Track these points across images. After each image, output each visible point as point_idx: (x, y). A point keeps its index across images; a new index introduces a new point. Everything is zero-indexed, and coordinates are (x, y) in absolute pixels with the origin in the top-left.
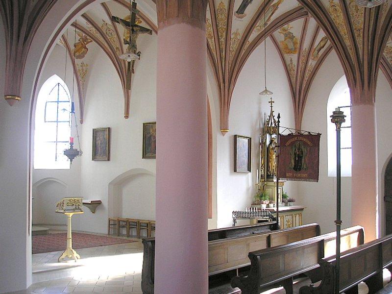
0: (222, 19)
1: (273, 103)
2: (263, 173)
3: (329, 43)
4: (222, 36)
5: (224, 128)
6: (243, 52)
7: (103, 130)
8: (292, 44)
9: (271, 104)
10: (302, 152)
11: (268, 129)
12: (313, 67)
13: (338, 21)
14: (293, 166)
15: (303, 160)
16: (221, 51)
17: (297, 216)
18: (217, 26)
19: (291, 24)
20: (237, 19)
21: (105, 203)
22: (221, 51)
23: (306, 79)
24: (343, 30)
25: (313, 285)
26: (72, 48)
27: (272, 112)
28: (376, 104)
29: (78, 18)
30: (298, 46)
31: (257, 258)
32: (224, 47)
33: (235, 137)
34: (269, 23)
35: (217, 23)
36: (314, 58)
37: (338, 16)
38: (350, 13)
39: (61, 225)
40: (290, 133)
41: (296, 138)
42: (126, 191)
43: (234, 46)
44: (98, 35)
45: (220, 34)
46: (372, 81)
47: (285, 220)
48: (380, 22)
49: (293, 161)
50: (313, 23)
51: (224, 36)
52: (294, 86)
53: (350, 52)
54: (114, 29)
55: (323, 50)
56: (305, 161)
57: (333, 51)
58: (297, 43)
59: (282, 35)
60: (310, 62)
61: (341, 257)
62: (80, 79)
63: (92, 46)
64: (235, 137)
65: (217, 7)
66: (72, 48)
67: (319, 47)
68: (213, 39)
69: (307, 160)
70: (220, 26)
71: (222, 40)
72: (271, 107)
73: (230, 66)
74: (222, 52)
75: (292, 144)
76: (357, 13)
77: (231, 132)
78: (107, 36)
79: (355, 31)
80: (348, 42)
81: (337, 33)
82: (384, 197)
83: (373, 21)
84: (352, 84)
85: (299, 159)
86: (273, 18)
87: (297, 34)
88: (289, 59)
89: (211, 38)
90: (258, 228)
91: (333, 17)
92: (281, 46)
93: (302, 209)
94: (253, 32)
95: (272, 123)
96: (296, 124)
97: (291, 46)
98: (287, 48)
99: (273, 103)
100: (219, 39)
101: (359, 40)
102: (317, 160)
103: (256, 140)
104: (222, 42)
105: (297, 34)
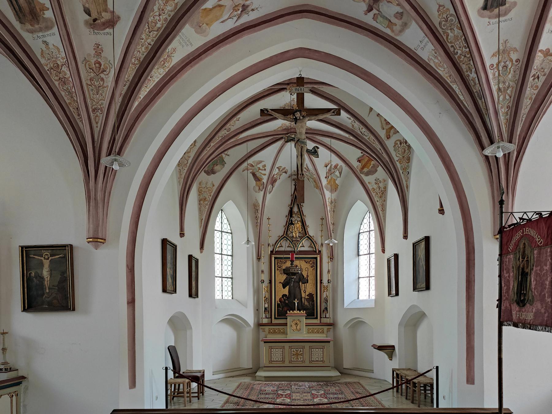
26: (356, 164)
58: (223, 163)
62: (376, 199)
66: (356, 164)
78: (364, 137)
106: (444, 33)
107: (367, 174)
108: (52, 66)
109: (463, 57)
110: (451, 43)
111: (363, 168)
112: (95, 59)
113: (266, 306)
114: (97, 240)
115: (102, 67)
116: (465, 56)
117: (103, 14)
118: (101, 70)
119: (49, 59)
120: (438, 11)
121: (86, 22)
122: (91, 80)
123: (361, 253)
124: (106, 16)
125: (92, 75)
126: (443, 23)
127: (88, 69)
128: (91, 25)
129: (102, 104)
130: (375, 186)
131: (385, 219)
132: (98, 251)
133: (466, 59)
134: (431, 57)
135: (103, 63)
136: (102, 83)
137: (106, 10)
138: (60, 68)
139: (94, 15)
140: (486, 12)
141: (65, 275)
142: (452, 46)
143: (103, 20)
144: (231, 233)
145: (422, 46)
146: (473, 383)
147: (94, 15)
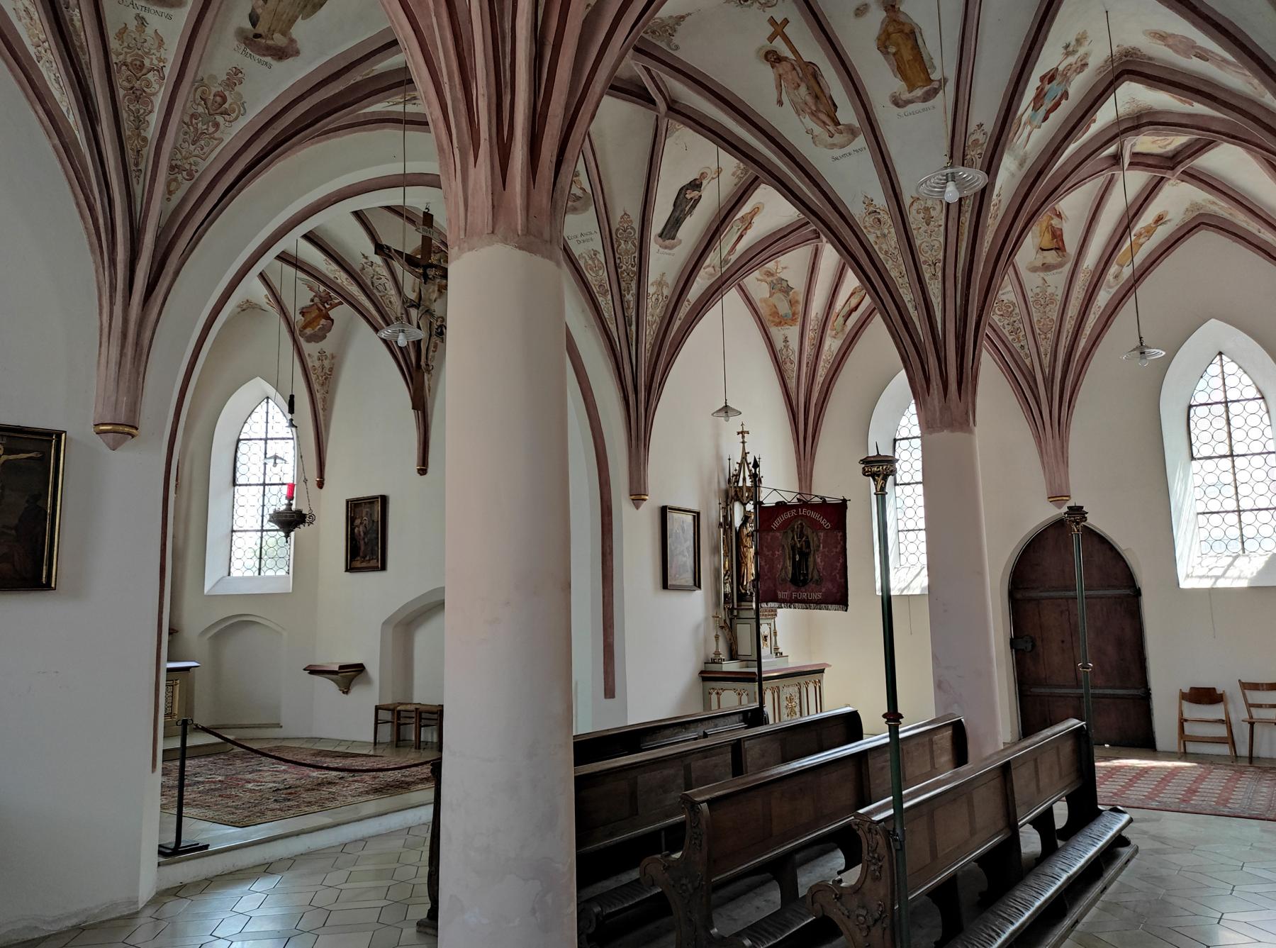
0: (627, 252)
2: (728, 590)
3: (867, 300)
5: (638, 496)
6: (677, 324)
7: (370, 501)
8: (786, 304)
10: (808, 543)
13: (884, 247)
15: (811, 559)
16: (627, 323)
19: (784, 260)
21: (373, 670)
23: (820, 379)
24: (896, 268)
25: (840, 881)
26: (299, 319)
27: (745, 454)
28: (976, 430)
29: (294, 242)
30: (800, 308)
31: (700, 811)
33: (664, 511)
34: (733, 258)
37: (884, 236)
38: (913, 226)
39: (260, 726)
41: (793, 512)
42: (423, 638)
43: (653, 312)
44: (354, 289)
45: (623, 284)
46: (966, 380)
47: (783, 697)
48: (980, 255)
49: (789, 564)
50: (830, 256)
51: (634, 291)
52: (793, 396)
53: (914, 314)
54: (389, 277)
56: (818, 560)
57: (878, 319)
58: (797, 302)
61: (901, 736)
62: (316, 387)
63: (341, 313)
64: (664, 511)
66: (299, 319)
67: (847, 309)
68: (609, 297)
69: (819, 560)
71: (630, 297)
75: (786, 525)
79: (924, 267)
80: (908, 296)
83: (968, 215)
84: (920, 391)
85: (802, 555)
86: (741, 247)
87: (797, 281)
88: (782, 339)
89: (604, 294)
90: (716, 721)
91: (872, 238)
92: (764, 311)
95: (744, 479)
96: (800, 480)
97: (784, 308)
100: (621, 296)
101: (934, 289)
103: (712, 514)
104: (628, 302)
105: (797, 281)
107: (309, 339)
108: (129, 60)
111: (305, 327)
112: (221, 89)
114: (122, 430)
115: (226, 105)
117: (277, 36)
118: (222, 109)
119: (129, 47)
121: (241, 33)
122: (193, 116)
123: (240, 480)
124: (279, 40)
125: (201, 110)
127: (198, 96)
128: (246, 38)
129: (196, 164)
130: (317, 364)
131: (327, 426)
132: (119, 454)
135: (229, 101)
136: (211, 130)
137: (284, 33)
138: (144, 71)
139: (261, 29)
141: (40, 503)
143: (270, 42)
144: (1263, 398)
146: (613, 696)
147: (261, 29)
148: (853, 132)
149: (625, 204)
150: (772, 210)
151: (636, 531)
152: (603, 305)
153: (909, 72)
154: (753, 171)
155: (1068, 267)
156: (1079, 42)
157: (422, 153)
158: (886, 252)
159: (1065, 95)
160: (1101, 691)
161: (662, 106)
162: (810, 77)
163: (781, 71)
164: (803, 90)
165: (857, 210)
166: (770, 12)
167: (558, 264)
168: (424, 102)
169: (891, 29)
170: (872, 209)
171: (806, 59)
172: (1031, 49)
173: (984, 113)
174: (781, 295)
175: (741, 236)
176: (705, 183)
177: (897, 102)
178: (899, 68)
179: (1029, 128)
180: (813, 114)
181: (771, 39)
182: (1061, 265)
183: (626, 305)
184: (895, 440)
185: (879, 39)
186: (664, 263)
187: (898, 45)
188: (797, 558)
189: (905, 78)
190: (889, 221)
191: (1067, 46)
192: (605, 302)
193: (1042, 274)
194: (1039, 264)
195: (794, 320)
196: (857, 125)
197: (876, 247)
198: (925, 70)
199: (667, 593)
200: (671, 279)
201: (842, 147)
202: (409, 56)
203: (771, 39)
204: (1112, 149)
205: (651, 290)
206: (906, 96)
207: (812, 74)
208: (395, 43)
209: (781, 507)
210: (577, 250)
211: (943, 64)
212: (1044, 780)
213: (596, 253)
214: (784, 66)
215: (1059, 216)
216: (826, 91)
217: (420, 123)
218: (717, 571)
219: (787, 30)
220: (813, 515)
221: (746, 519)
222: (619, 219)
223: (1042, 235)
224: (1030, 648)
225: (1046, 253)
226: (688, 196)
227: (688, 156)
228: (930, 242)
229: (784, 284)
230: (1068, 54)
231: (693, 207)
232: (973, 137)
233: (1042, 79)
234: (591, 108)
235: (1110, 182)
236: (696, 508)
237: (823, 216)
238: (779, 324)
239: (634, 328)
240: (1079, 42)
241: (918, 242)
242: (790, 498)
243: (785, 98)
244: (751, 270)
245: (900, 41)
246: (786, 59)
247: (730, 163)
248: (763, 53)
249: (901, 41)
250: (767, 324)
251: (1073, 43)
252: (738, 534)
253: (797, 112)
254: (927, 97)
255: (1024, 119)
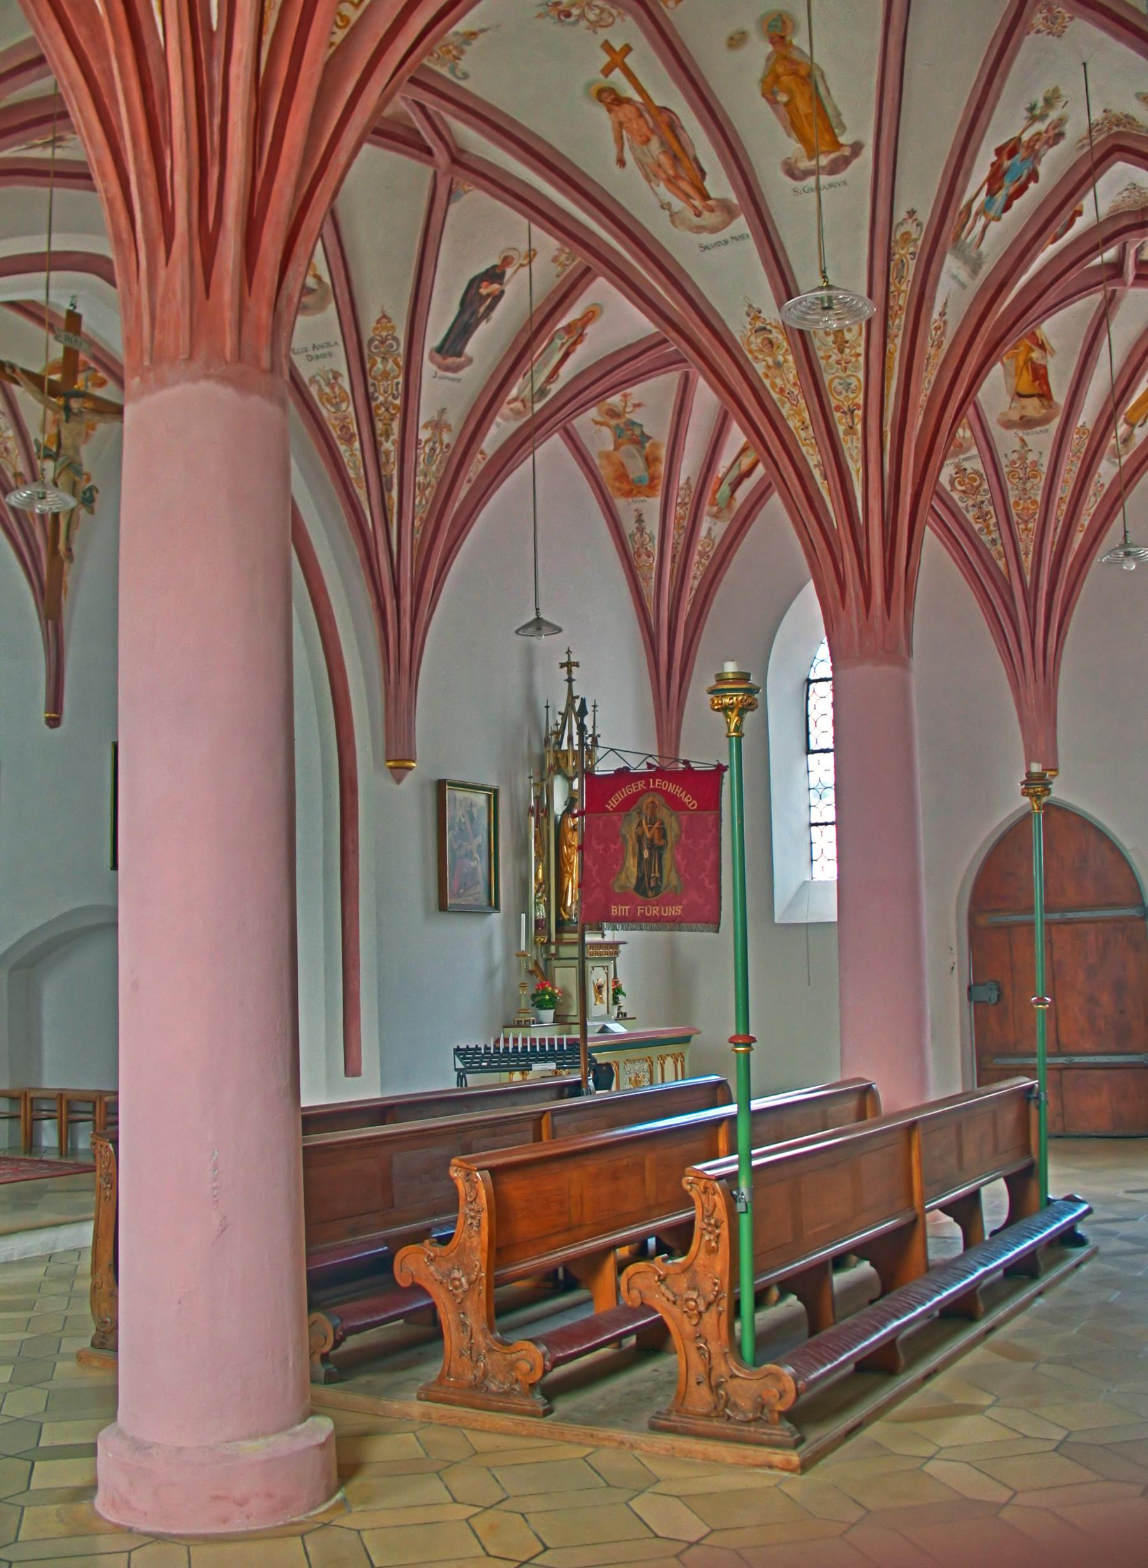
0: (386, 375)
1: (574, 669)
2: (542, 913)
4: (387, 434)
5: (398, 760)
6: (463, 490)
8: (640, 463)
9: (570, 672)
11: (557, 759)
12: (717, 541)
13: (779, 382)
14: (633, 881)
17: (669, 1062)
18: (368, 398)
19: (636, 391)
20: (441, 373)
22: (384, 487)
24: (797, 417)
27: (571, 698)
28: (915, 662)
30: (662, 468)
32: (395, 472)
33: (441, 786)
34: (555, 388)
35: (371, 389)
36: (720, 511)
37: (778, 365)
38: (820, 354)
40: (622, 765)
41: (641, 785)
43: (428, 470)
45: (379, 426)
46: (899, 583)
55: (748, 485)
59: (607, 433)
60: (705, 524)
64: (441, 786)
65: (368, 333)
67: (735, 473)
68: (357, 445)
70: (381, 399)
71: (389, 446)
72: (570, 680)
73: (418, 536)
74: (390, 490)
75: (628, 804)
76: (841, 351)
77: (421, 771)
79: (837, 415)
81: (779, 424)
82: (969, 989)
83: (898, 341)
86: (567, 372)
89: (349, 440)
91: (760, 368)
92: (605, 472)
93: (686, 1040)
94: (498, 419)
95: (570, 739)
97: (637, 469)
98: (622, 476)
99: (574, 669)
101: (851, 448)
102: (712, 857)
104: (387, 453)
106: (370, 358)
109: (383, 409)
110: (374, 378)
113: (542, 913)
116: (387, 410)
120: (378, 322)
126: (376, 343)
133: (387, 415)
134: (318, 378)
140: (438, 357)
142: (373, 385)
145: (312, 353)
148: (729, 212)
149: (383, 300)
150: (616, 319)
151: (393, 813)
152: (346, 457)
153: (807, 130)
154: (582, 258)
155: (1056, 422)
156: (1049, 102)
157: (84, 223)
158: (782, 391)
159: (1034, 176)
160: (1091, 1059)
161: (442, 157)
162: (664, 127)
163: (622, 118)
164: (655, 145)
165: (738, 327)
166: (603, 34)
167: (283, 404)
168: (82, 144)
169: (780, 69)
170: (759, 324)
171: (658, 102)
172: (979, 109)
173: (917, 196)
174: (632, 448)
175: (566, 355)
176: (509, 271)
177: (792, 171)
178: (793, 124)
179: (982, 220)
180: (671, 182)
181: (607, 71)
182: (1046, 420)
183: (383, 459)
184: (809, 682)
185: (763, 81)
186: (443, 394)
187: (790, 92)
188: (646, 854)
189: (803, 139)
190: (785, 344)
191: (1032, 109)
192: (351, 454)
193: (1020, 433)
194: (1015, 416)
195: (652, 486)
196: (735, 201)
197: (767, 382)
198: (830, 129)
199: (444, 915)
200: (455, 418)
201: (714, 230)
202: (63, 76)
203: (607, 71)
204: (1110, 254)
205: (424, 435)
206: (806, 164)
207: (670, 125)
208: (40, 60)
209: (623, 775)
210: (306, 371)
211: (858, 125)
212: (970, 1154)
213: (336, 375)
214: (627, 112)
215: (1042, 347)
216: (689, 150)
217: (76, 175)
218: (525, 884)
219: (629, 60)
220: (672, 788)
221: (571, 803)
222: (373, 324)
223: (1019, 375)
224: (994, 996)
225: (1025, 401)
226: (484, 291)
227: (484, 233)
228: (845, 382)
229: (637, 432)
230: (1033, 119)
231: (491, 308)
232: (902, 230)
233: (999, 152)
234: (333, 185)
235: (1110, 302)
236: (493, 783)
237: (690, 334)
238: (628, 494)
239: (395, 493)
240: (1049, 102)
241: (827, 378)
242: (637, 764)
243: (628, 155)
244: (584, 406)
245: (793, 86)
246: (629, 101)
247: (548, 244)
248: (594, 90)
249: (794, 84)
250: (610, 491)
251: (1041, 103)
252: (560, 827)
253: (647, 178)
254: (835, 168)
255: (975, 207)
